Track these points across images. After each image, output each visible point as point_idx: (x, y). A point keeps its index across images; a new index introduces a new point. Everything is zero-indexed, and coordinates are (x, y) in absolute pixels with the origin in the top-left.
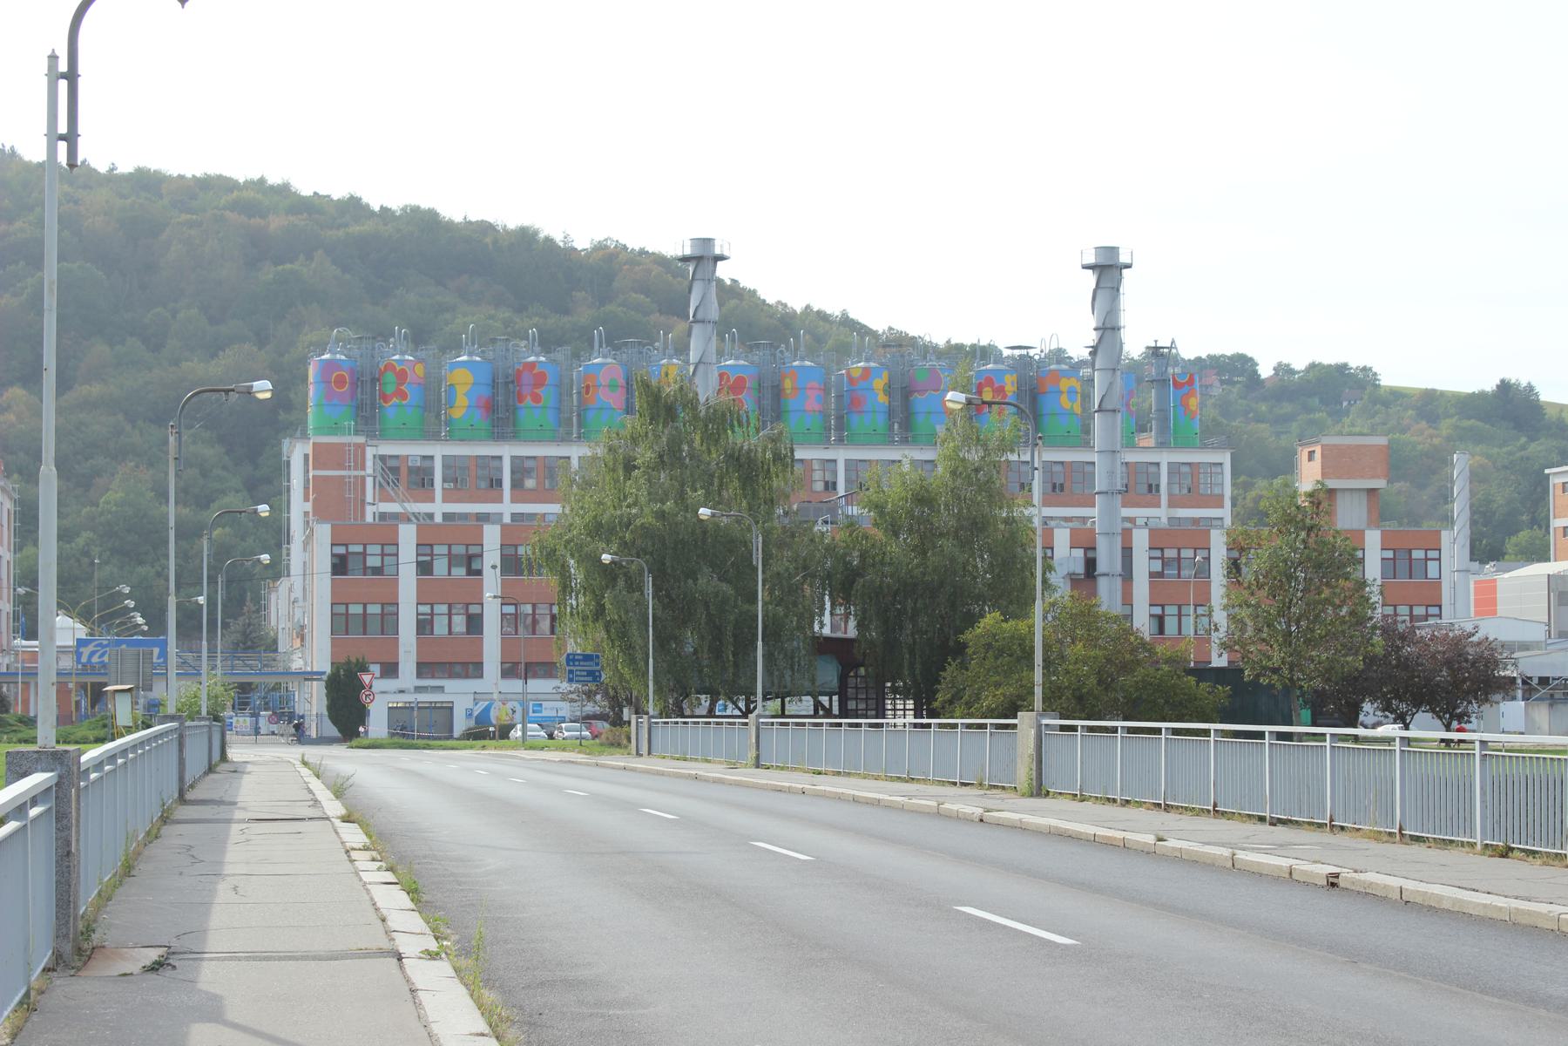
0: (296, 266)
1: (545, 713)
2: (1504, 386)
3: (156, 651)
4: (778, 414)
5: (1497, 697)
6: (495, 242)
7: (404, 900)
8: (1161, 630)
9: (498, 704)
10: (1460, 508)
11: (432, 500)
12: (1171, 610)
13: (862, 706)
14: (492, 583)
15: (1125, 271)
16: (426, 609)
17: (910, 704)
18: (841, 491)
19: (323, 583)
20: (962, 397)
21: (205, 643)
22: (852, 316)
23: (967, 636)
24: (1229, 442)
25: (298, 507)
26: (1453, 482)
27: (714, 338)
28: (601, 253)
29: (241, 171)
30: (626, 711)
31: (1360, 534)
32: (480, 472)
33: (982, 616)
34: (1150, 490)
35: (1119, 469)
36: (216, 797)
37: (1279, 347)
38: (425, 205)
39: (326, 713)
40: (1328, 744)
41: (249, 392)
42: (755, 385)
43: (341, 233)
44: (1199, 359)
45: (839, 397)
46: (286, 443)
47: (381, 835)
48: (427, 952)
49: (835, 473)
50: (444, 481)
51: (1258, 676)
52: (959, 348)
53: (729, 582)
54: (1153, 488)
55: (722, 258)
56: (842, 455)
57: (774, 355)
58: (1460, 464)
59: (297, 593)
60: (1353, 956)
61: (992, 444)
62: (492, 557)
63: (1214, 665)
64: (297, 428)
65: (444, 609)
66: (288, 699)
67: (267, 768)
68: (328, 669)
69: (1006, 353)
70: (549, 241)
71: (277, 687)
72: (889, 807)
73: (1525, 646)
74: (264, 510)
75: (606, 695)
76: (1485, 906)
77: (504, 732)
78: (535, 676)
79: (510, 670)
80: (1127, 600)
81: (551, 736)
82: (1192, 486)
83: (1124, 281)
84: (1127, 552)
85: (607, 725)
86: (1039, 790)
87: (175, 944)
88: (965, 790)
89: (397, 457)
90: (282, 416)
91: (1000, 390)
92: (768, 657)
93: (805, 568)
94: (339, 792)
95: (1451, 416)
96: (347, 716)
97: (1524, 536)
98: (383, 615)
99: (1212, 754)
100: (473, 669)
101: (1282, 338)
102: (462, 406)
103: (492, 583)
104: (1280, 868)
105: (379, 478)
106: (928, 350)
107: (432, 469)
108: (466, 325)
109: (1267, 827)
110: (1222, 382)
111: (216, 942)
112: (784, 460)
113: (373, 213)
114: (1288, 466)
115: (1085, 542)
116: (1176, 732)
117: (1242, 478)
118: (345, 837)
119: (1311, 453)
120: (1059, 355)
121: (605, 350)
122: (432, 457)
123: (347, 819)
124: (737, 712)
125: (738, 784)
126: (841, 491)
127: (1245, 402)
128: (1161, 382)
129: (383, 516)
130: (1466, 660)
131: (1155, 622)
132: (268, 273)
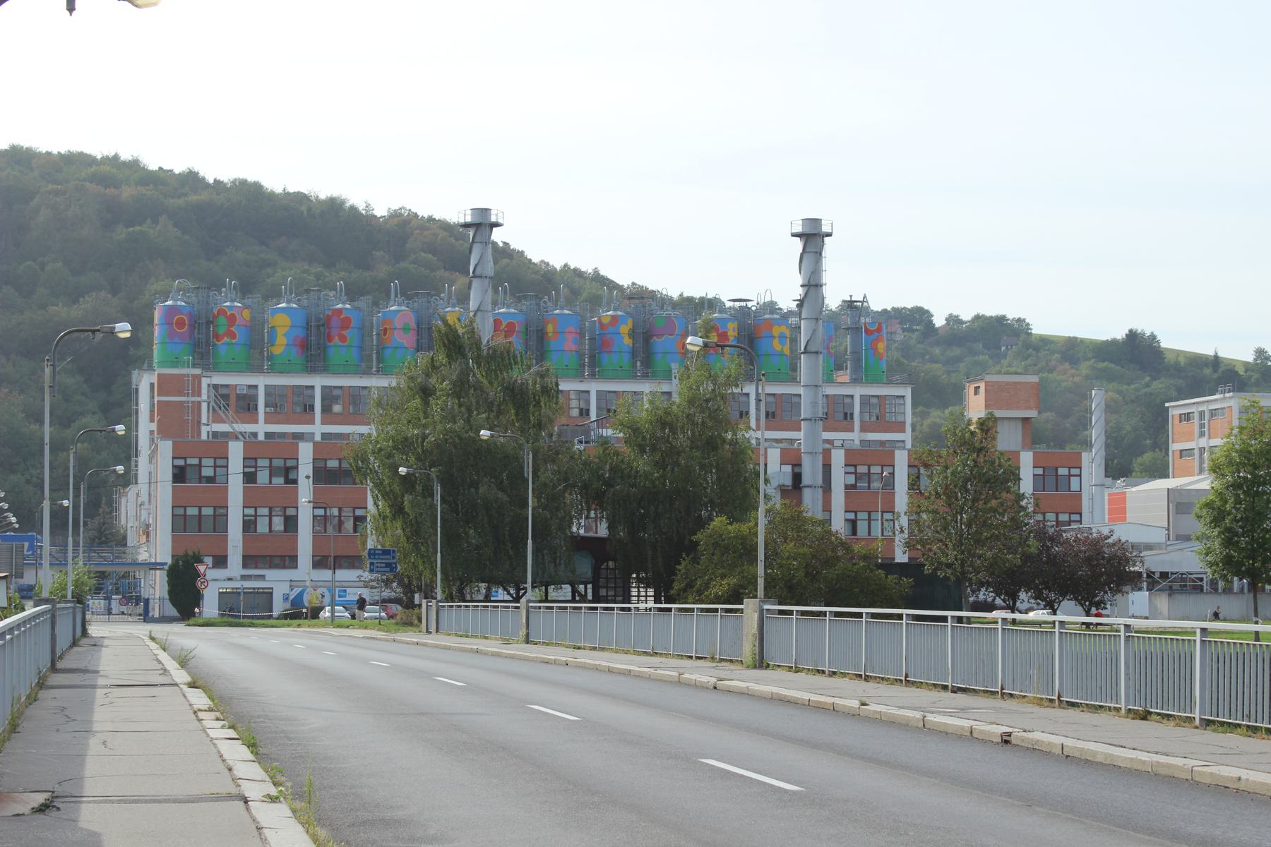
0: (144, 228)
1: (348, 598)
2: (1132, 336)
3: (26, 545)
4: (542, 355)
5: (1125, 588)
6: (309, 210)
7: (245, 753)
8: (854, 532)
9: (309, 590)
10: (1097, 433)
11: (256, 422)
12: (862, 516)
13: (611, 593)
14: (305, 491)
15: (826, 239)
16: (251, 511)
17: (651, 592)
18: (593, 416)
19: (165, 491)
20: (700, 341)
21: (70, 539)
22: (602, 273)
23: (699, 536)
24: (911, 379)
25: (145, 427)
26: (1091, 413)
27: (490, 291)
28: (396, 220)
29: (98, 149)
30: (417, 596)
31: (1017, 454)
32: (296, 399)
33: (712, 520)
34: (845, 418)
35: (821, 401)
36: (82, 666)
37: (951, 299)
38: (251, 178)
39: (167, 596)
40: (1057, 630)
41: (112, 332)
42: (523, 329)
43: (181, 201)
44: (885, 311)
45: (592, 339)
46: (135, 373)
47: (221, 698)
48: (269, 796)
49: (588, 402)
50: (266, 406)
51: (936, 570)
52: (690, 300)
53: (503, 490)
54: (848, 416)
55: (497, 225)
56: (594, 387)
57: (538, 305)
58: (1097, 398)
59: (144, 497)
60: (1028, 800)
61: (721, 379)
62: (305, 469)
63: (898, 560)
64: (144, 361)
65: (265, 511)
66: (136, 585)
67: (121, 642)
68: (169, 560)
69: (728, 304)
70: (353, 209)
71: (126, 575)
72: (638, 676)
73: (1149, 547)
74: (120, 429)
75: (401, 583)
76: (1132, 759)
77: (315, 613)
78: (341, 567)
79: (320, 562)
80: (827, 507)
81: (353, 617)
82: (880, 415)
83: (826, 247)
84: (827, 468)
85: (399, 608)
86: (761, 663)
87: (58, 789)
88: (700, 663)
89: (227, 386)
90: (132, 351)
91: (723, 336)
92: (535, 552)
93: (566, 479)
94: (183, 663)
95: (1089, 359)
96: (185, 600)
97: (1147, 457)
98: (215, 516)
99: (904, 635)
100: (288, 560)
101: (954, 296)
102: (281, 345)
103: (305, 491)
104: (962, 728)
105: (212, 403)
106: (664, 301)
107: (257, 395)
108: (285, 278)
109: (949, 694)
110: (904, 330)
111: (91, 788)
112: (550, 392)
113: (208, 184)
114: (957, 396)
115: (792, 459)
116: (874, 616)
117: (920, 408)
118: (193, 700)
119: (977, 389)
120: (771, 307)
121: (400, 299)
122: (256, 387)
123: (193, 685)
124: (508, 598)
125: (512, 657)
126: (593, 416)
127: (921, 346)
128: (855, 330)
129: (215, 434)
130: (1103, 558)
131: (849, 526)
132: (121, 233)
